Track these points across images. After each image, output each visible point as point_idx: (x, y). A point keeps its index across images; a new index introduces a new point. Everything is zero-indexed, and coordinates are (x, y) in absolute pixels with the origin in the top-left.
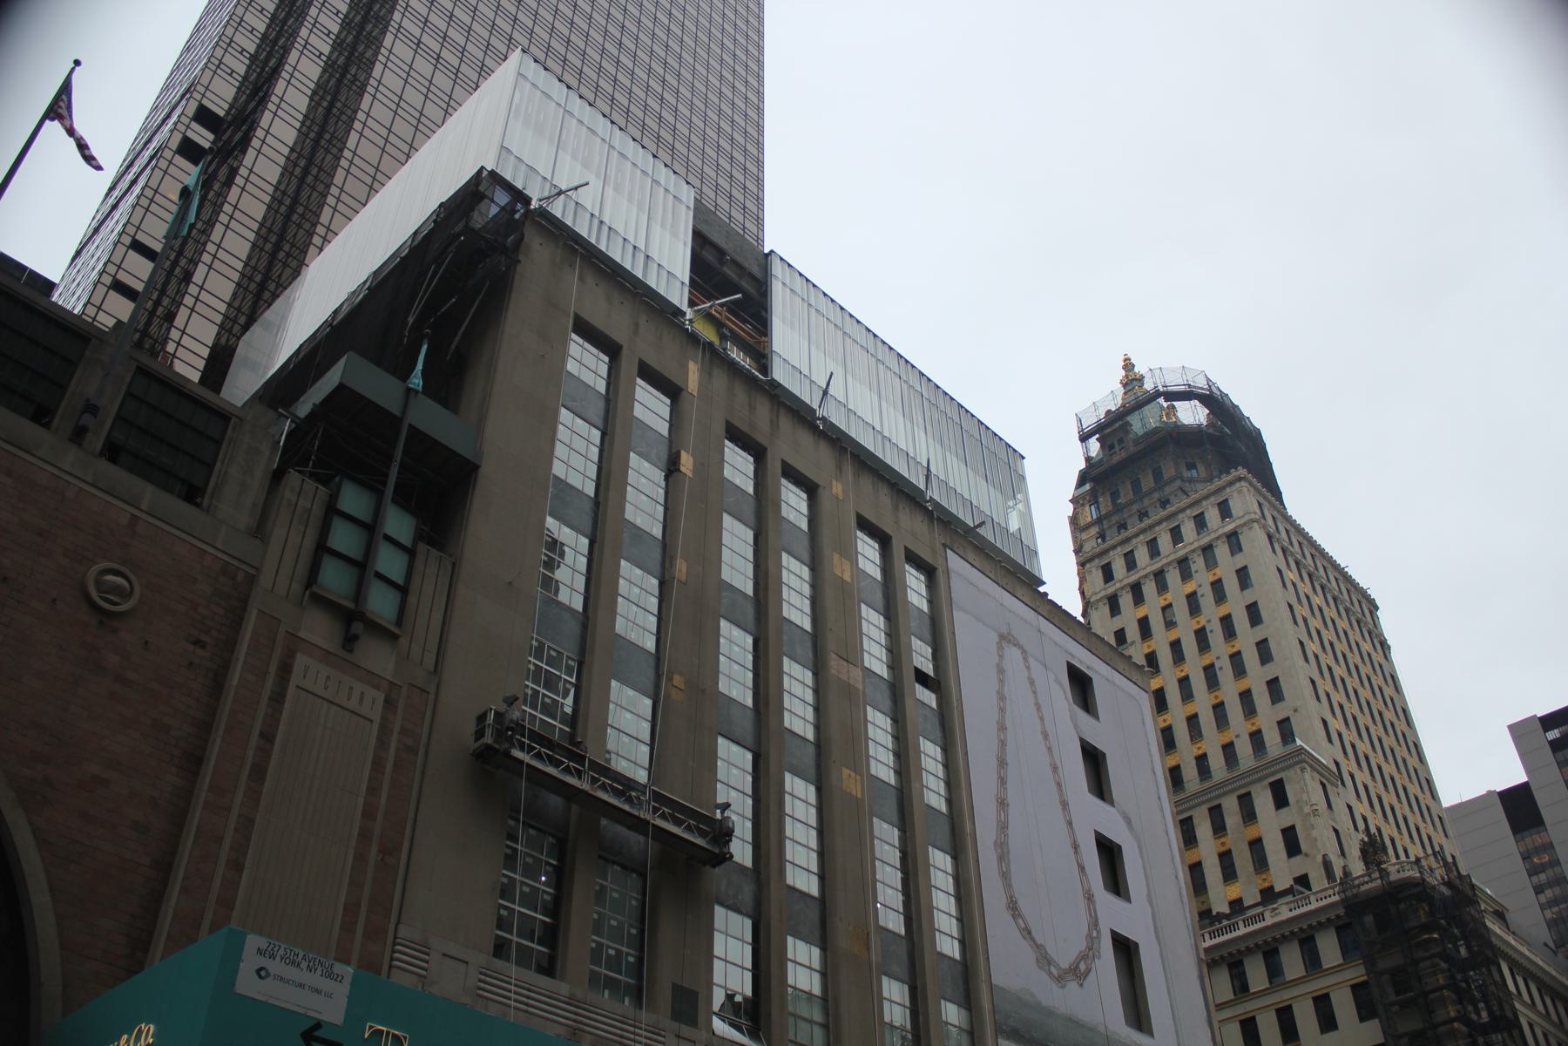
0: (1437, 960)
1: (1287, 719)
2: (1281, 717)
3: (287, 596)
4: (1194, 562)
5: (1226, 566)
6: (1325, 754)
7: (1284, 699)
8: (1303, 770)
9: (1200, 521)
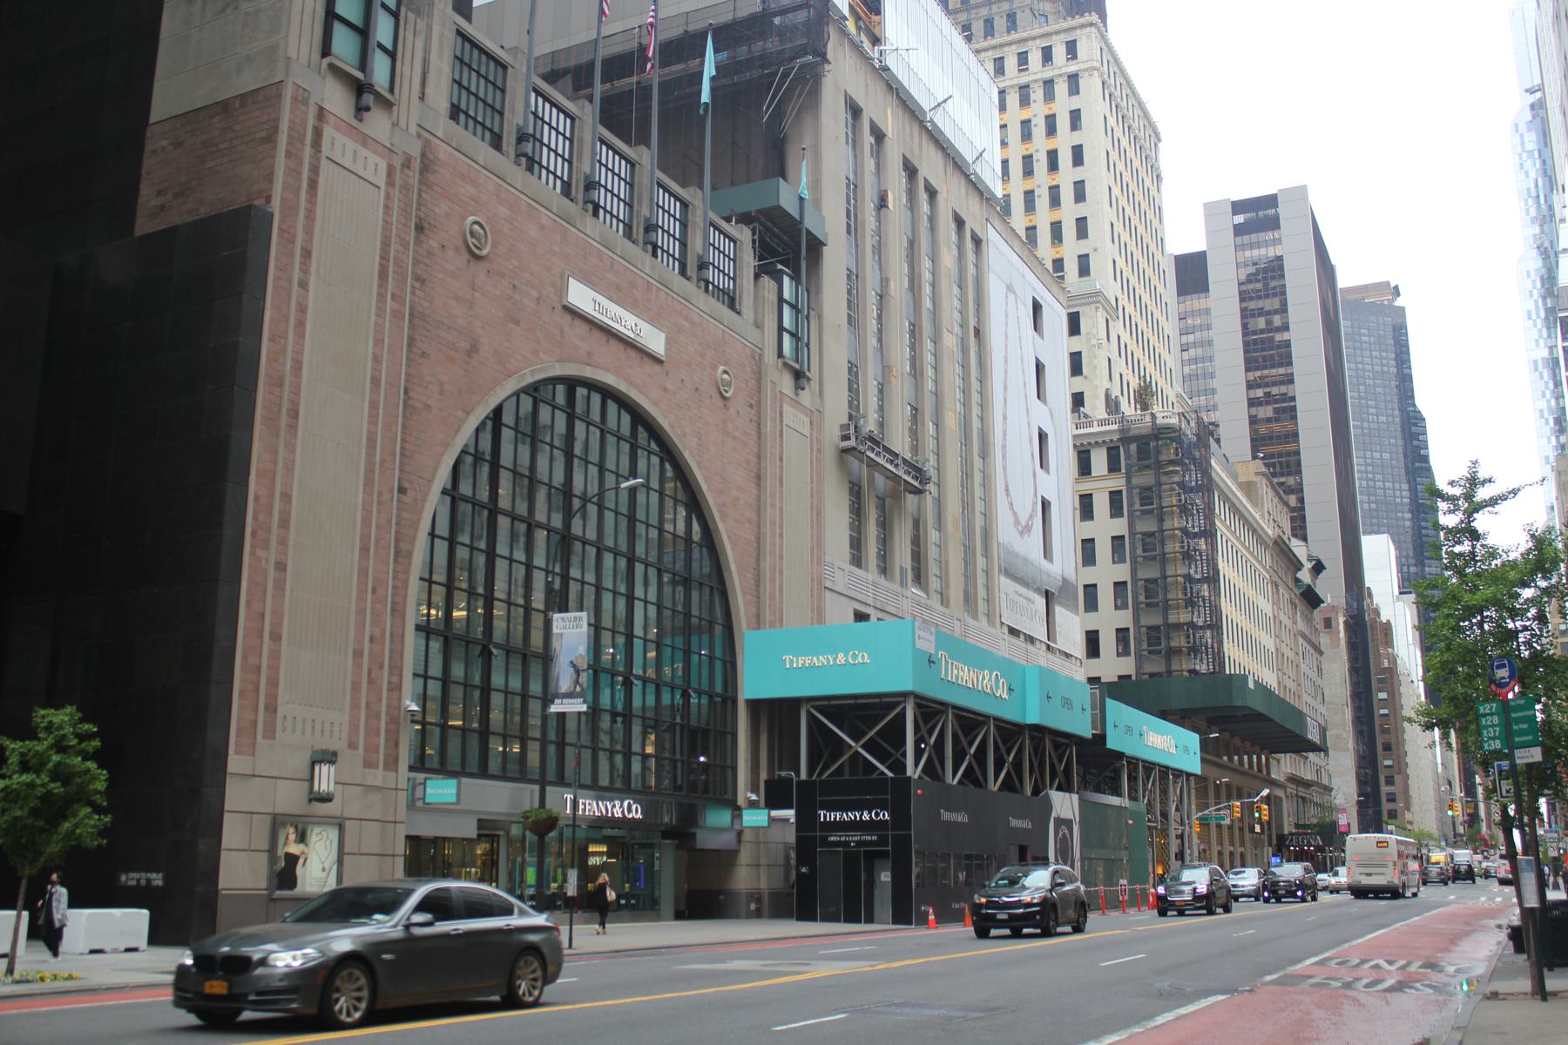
0: (1175, 486)
1: (1087, 255)
2: (1083, 252)
3: (309, 66)
4: (1034, 92)
5: (1063, 104)
6: (1112, 290)
7: (1087, 237)
8: (1097, 308)
9: (1047, 55)
